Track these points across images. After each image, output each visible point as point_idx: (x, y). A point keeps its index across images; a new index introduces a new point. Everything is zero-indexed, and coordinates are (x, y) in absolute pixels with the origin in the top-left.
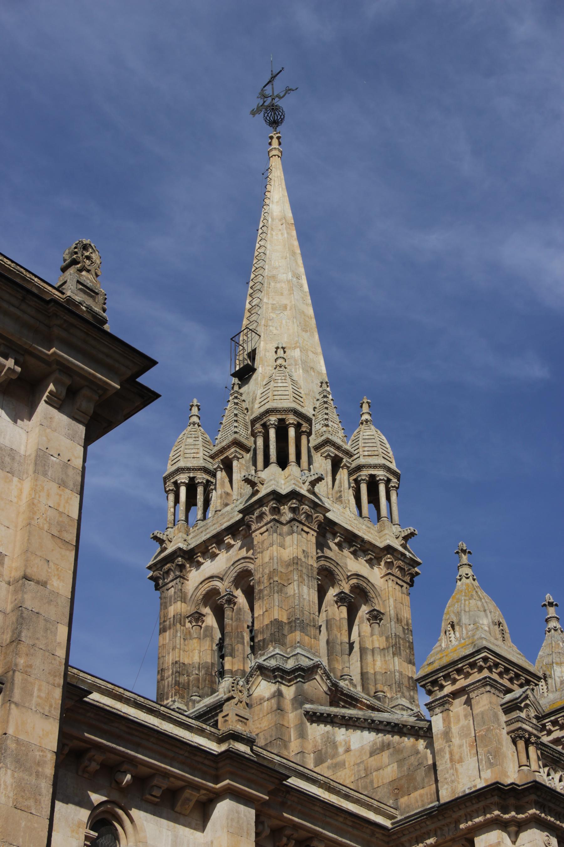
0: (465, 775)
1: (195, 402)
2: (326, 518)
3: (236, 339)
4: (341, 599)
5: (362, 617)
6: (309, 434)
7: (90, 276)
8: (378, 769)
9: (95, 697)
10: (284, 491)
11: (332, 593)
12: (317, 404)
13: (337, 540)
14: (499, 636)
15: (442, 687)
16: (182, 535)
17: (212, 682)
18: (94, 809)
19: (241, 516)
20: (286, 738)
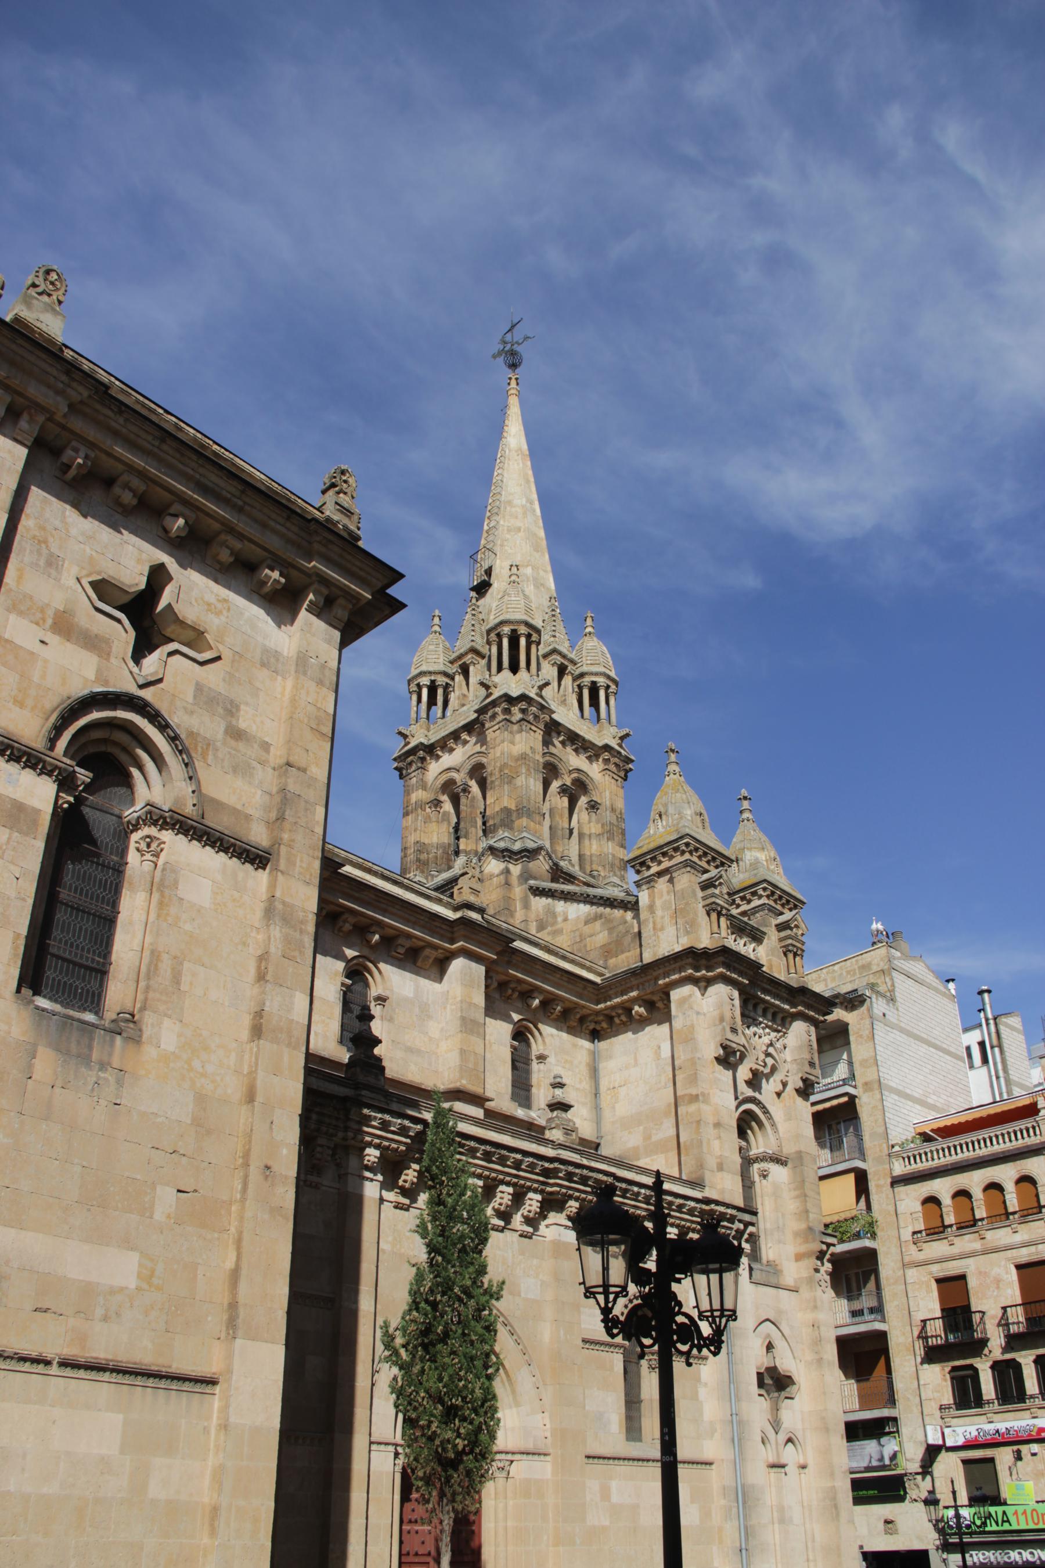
0: (666, 941)
1: (437, 613)
2: (551, 719)
3: (474, 557)
4: (564, 790)
5: (581, 807)
6: (538, 643)
7: (347, 499)
8: (591, 936)
9: (348, 869)
10: (515, 693)
11: (555, 785)
12: (546, 617)
13: (561, 739)
14: (700, 825)
15: (649, 868)
16: (424, 731)
17: (449, 860)
18: (348, 961)
19: (476, 715)
20: (512, 909)
